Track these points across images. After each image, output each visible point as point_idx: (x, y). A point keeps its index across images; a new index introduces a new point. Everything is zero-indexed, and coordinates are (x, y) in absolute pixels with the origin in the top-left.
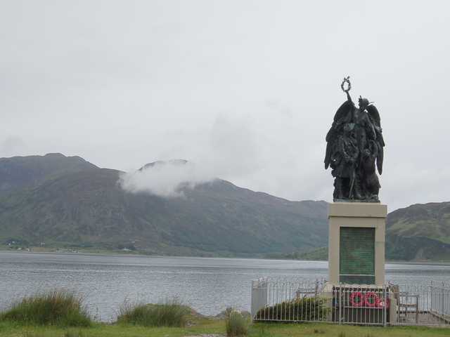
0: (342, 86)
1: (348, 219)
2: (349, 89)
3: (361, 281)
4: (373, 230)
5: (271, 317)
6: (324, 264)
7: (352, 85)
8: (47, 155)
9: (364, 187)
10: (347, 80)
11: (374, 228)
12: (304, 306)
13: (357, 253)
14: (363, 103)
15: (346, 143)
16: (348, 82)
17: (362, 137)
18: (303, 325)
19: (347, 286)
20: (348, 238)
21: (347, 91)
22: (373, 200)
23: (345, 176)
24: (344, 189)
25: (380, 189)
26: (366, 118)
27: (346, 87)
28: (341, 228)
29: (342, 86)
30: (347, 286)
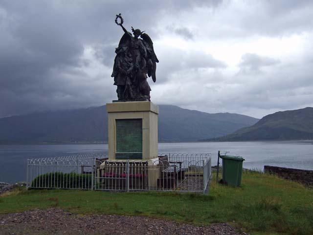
0: (116, 21)
1: (142, 113)
2: (122, 22)
3: (132, 157)
4: (140, 120)
5: (41, 186)
6: (105, 147)
7: (124, 20)
8: (307, 108)
9: (138, 91)
10: (119, 16)
11: (141, 119)
12: (50, 176)
13: (129, 137)
14: (137, 32)
15: (121, 61)
16: (121, 18)
17: (137, 56)
18: (68, 191)
19: (121, 161)
20: (122, 127)
21: (121, 25)
22: (141, 99)
23: (122, 84)
24: (124, 93)
25: (151, 92)
26: (140, 43)
27: (119, 21)
28: (116, 120)
29: (116, 21)
30: (121, 161)
